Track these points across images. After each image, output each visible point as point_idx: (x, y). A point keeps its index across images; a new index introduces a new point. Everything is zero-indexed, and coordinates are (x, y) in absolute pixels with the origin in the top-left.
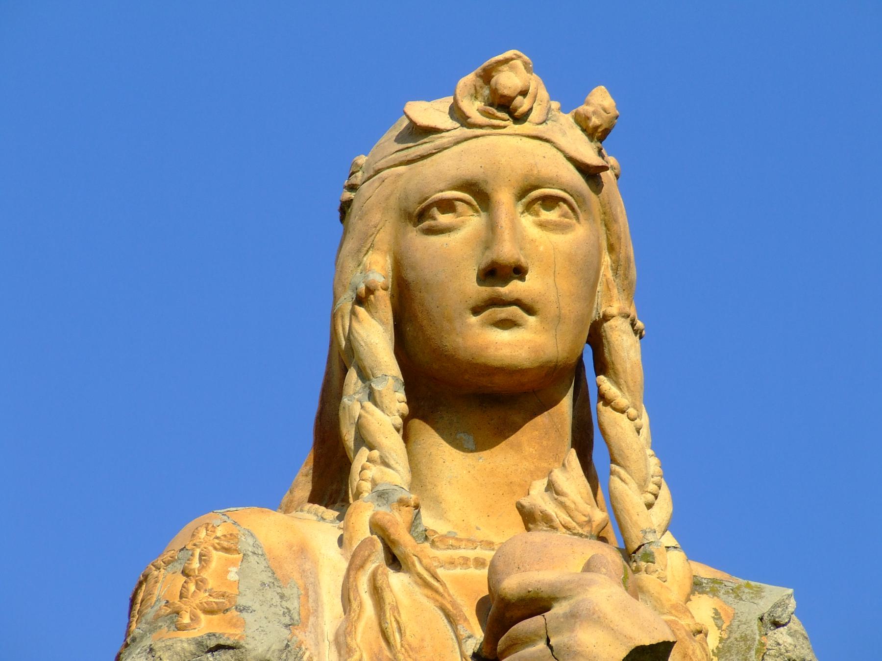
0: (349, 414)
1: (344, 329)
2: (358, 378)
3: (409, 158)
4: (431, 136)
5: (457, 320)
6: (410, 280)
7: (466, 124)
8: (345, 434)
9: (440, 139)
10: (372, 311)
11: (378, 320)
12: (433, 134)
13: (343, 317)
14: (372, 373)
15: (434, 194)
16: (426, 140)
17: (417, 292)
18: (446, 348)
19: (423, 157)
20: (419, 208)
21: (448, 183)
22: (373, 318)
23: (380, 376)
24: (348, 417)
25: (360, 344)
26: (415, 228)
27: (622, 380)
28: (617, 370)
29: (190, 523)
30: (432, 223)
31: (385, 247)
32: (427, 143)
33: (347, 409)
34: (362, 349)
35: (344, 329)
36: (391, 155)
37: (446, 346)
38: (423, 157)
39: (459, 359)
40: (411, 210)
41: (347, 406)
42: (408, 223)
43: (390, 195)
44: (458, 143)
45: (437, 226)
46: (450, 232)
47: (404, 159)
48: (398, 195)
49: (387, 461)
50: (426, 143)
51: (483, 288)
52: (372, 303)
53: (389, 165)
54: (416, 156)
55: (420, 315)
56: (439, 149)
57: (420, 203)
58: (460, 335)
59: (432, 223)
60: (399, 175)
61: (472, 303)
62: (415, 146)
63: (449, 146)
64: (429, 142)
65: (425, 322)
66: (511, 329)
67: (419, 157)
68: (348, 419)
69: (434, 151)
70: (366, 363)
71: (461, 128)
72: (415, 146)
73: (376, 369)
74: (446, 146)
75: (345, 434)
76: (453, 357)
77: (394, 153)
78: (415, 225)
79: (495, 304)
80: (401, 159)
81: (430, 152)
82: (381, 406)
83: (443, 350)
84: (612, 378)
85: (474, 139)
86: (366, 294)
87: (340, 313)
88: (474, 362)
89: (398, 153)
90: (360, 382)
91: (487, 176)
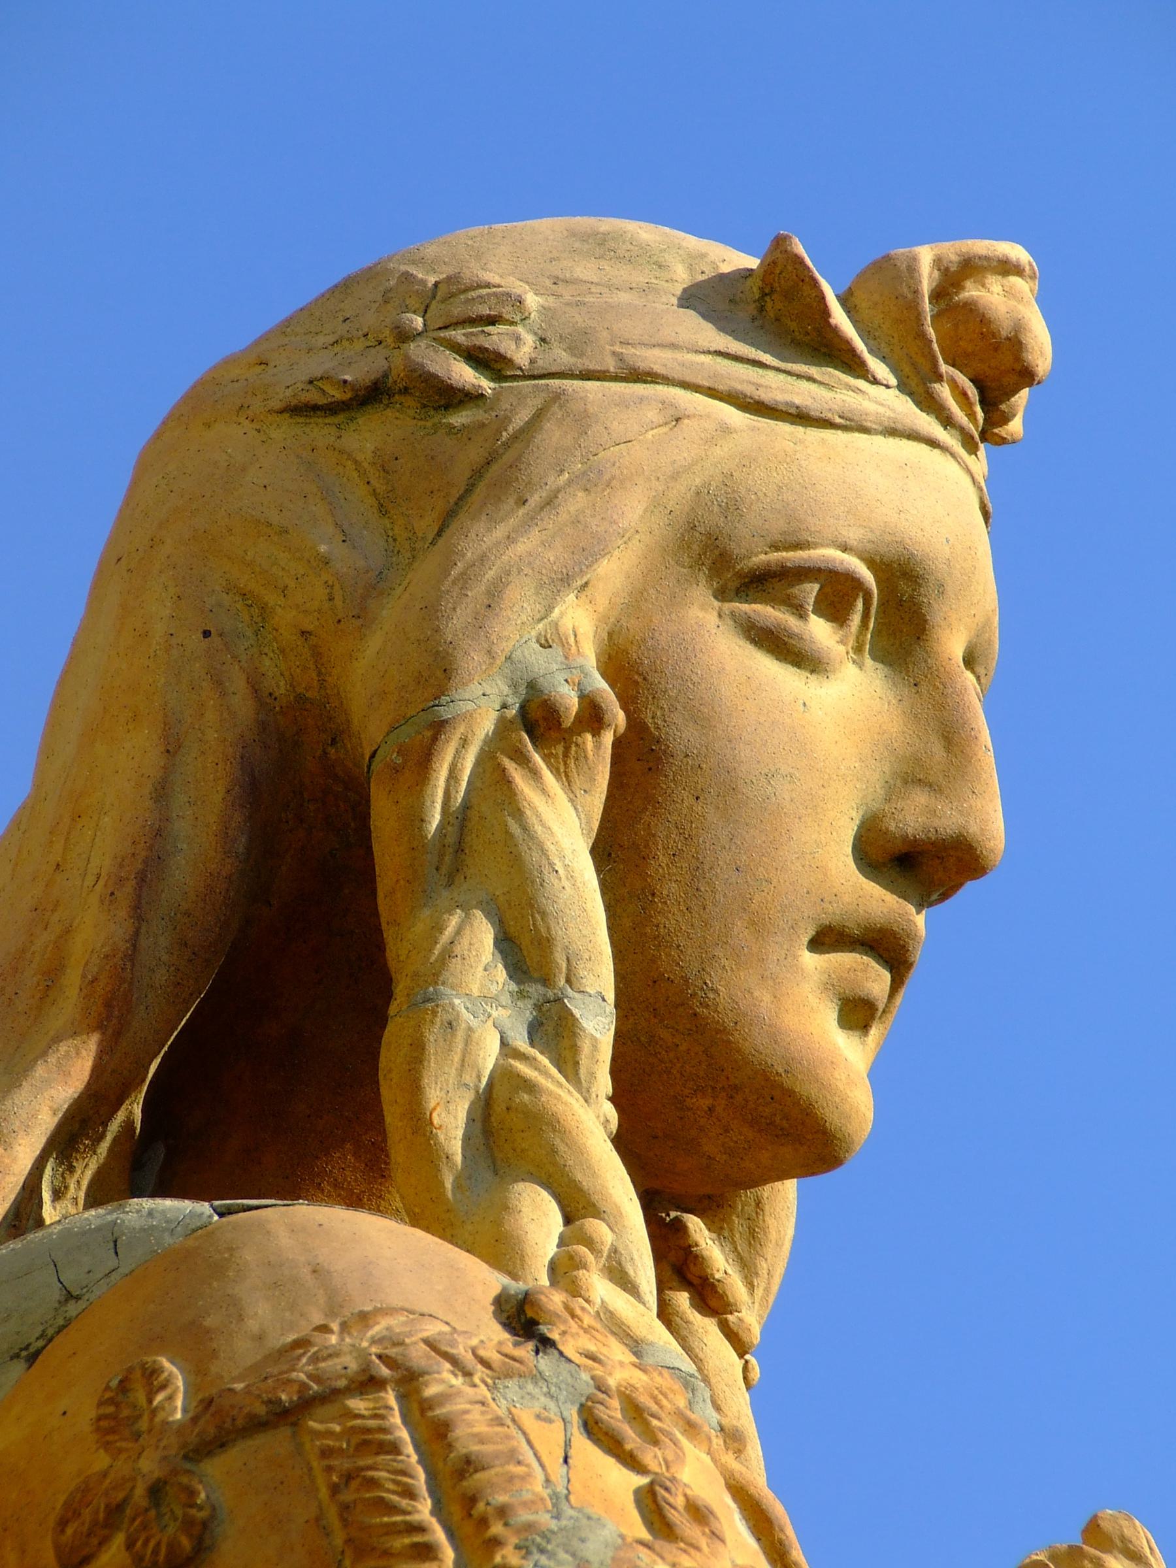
0: (465, 1053)
1: (453, 776)
2: (499, 956)
3: (765, 396)
4: (830, 370)
5: (779, 939)
6: (677, 747)
7: (921, 390)
8: (432, 1105)
9: (851, 393)
10: (578, 782)
11: (583, 816)
12: (836, 368)
13: (464, 743)
14: (569, 970)
15: (828, 546)
16: (813, 371)
17: (685, 794)
18: (711, 996)
19: (801, 417)
20: (763, 557)
21: (870, 536)
22: (571, 801)
23: (592, 992)
24: (457, 1058)
25: (551, 865)
26: (716, 604)
27: (765, 1266)
28: (765, 1230)
29: (485, 1266)
30: (790, 621)
31: (602, 603)
32: (814, 381)
33: (460, 1035)
34: (556, 882)
35: (453, 776)
36: (696, 352)
37: (716, 991)
38: (801, 417)
39: (739, 1051)
40: (736, 550)
41: (463, 1026)
42: (702, 579)
43: (688, 469)
44: (892, 432)
45: (801, 638)
46: (812, 672)
47: (749, 390)
48: (698, 481)
49: (631, 1273)
50: (810, 379)
51: (873, 889)
52: (586, 757)
53: (689, 378)
54: (787, 403)
55: (663, 860)
56: (850, 420)
57: (775, 547)
58: (770, 982)
59: (790, 621)
60: (726, 430)
61: (832, 913)
62: (778, 370)
63: (874, 426)
64: (821, 383)
65: (671, 889)
66: (851, 1033)
67: (793, 411)
68: (456, 1064)
69: (838, 420)
70: (558, 932)
71: (897, 392)
72: (778, 370)
73: (589, 966)
74: (869, 424)
75: (432, 1105)
76: (718, 1032)
77: (709, 352)
78: (721, 594)
79: (872, 948)
80: (739, 387)
81: (829, 415)
82: (584, 1084)
83: (694, 995)
84: (734, 1243)
85: (924, 446)
86: (573, 723)
87: (461, 729)
88: (787, 1082)
89: (719, 359)
90: (501, 974)
91: (950, 574)
